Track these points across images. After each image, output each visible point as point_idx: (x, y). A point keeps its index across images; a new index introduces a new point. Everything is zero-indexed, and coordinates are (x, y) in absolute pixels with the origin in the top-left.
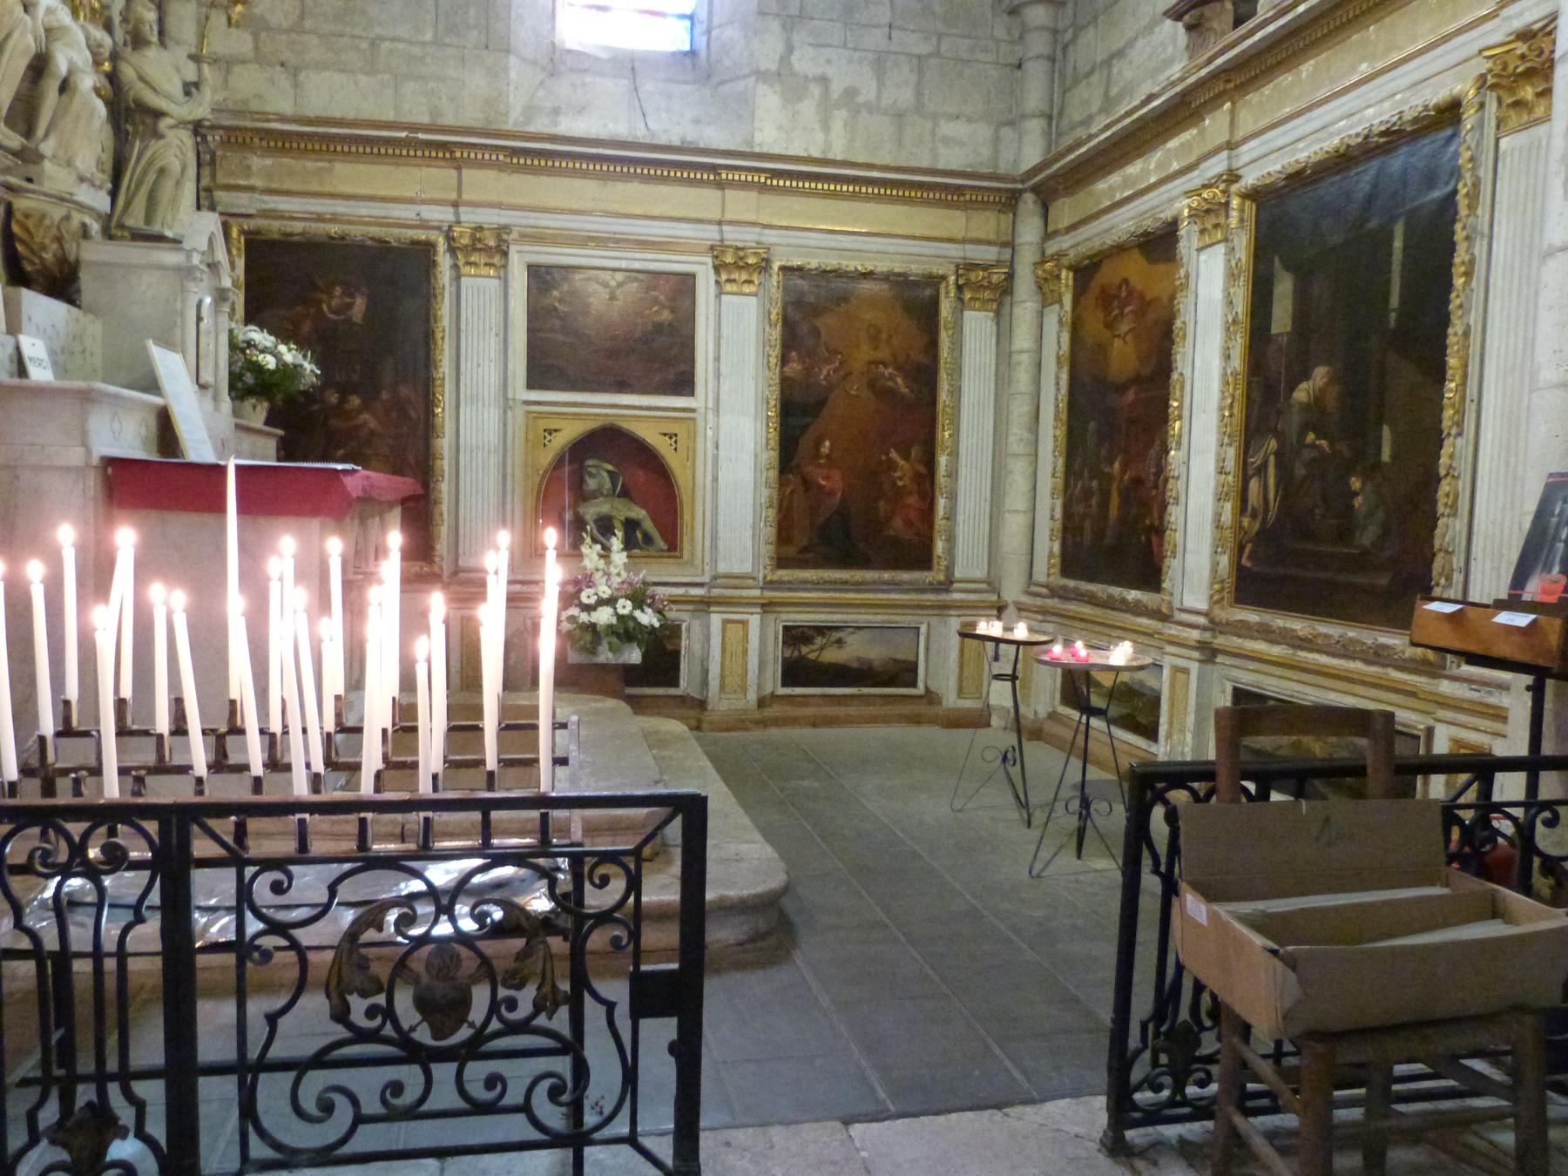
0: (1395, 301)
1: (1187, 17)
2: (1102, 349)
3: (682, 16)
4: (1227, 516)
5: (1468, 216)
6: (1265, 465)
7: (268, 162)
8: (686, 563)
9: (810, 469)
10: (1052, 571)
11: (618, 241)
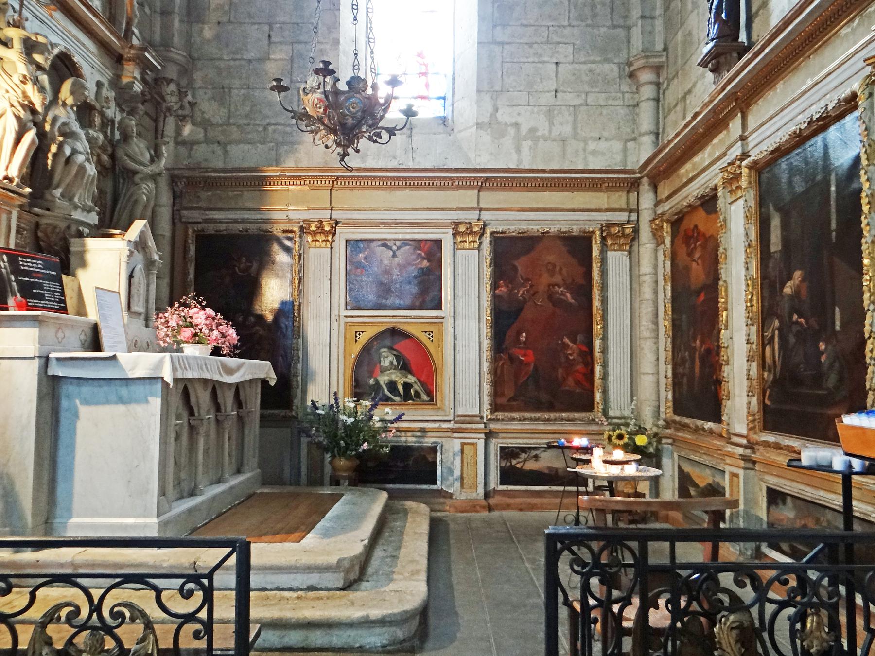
0: (834, 226)
1: (710, 65)
2: (687, 269)
3: (439, 98)
4: (754, 372)
5: (868, 165)
6: (773, 337)
7: (210, 194)
8: (439, 409)
9: (515, 351)
10: (668, 411)
11: (397, 224)
